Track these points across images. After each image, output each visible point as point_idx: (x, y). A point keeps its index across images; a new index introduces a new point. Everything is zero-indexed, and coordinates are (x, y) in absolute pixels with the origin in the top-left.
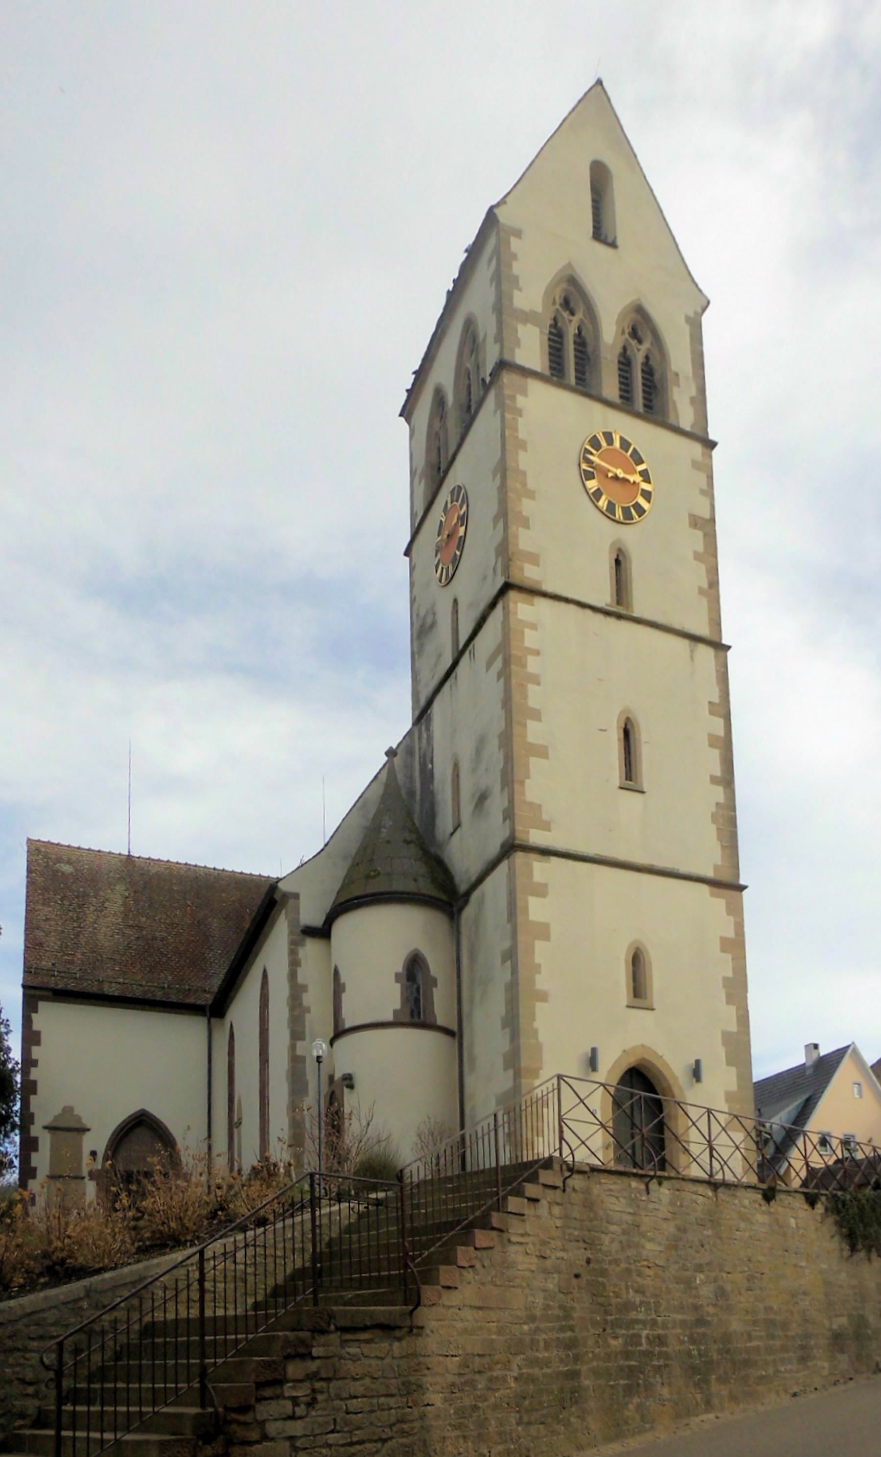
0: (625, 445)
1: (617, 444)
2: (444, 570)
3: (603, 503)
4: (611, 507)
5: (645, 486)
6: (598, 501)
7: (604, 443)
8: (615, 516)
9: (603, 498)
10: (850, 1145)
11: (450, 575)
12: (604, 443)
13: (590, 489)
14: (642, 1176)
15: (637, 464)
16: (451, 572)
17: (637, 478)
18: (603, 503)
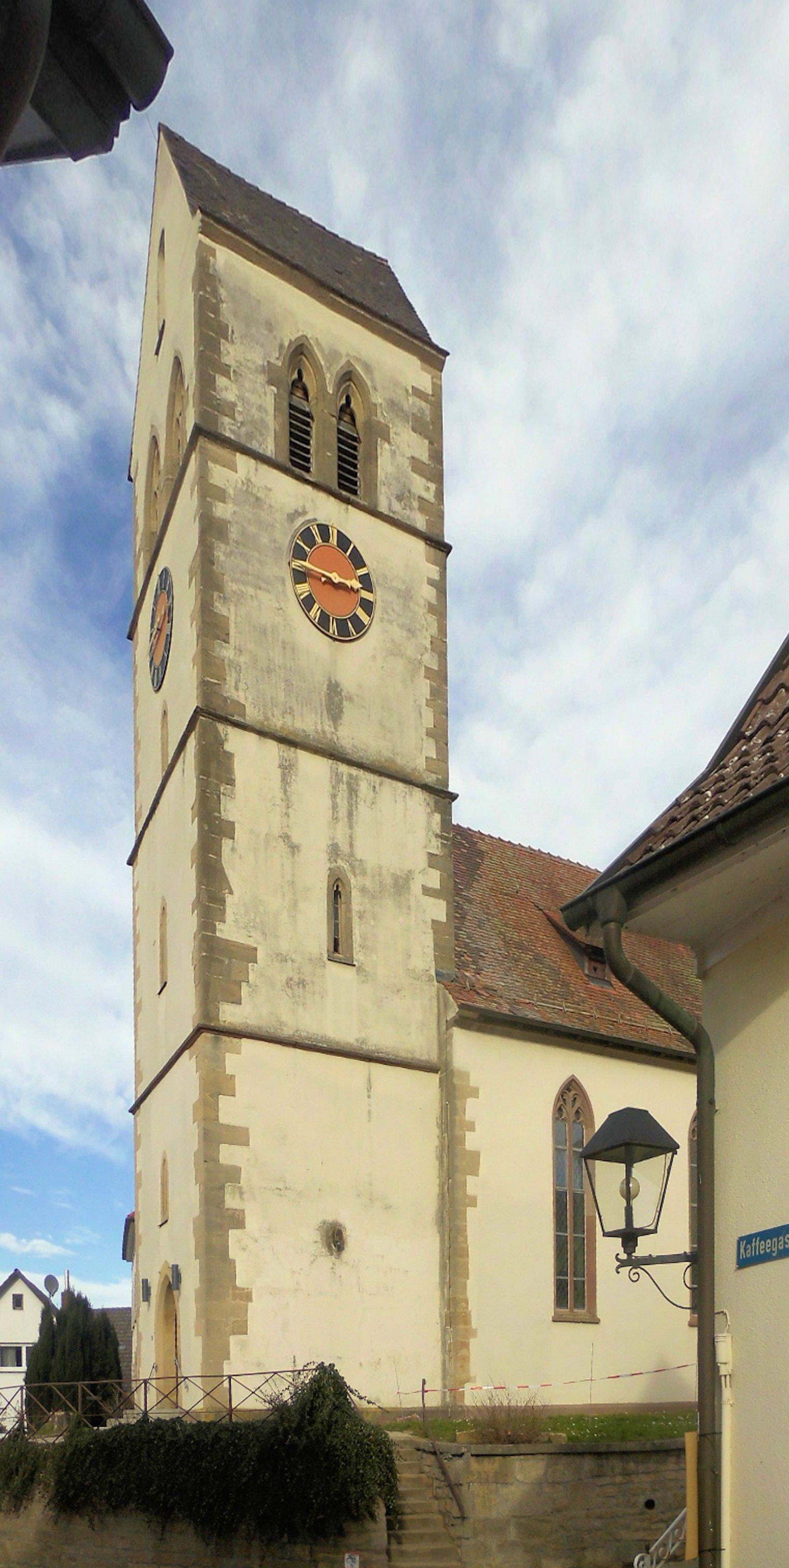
0: (343, 541)
1: (334, 540)
2: (156, 671)
3: (315, 612)
4: (326, 537)
5: (365, 594)
6: (309, 612)
7: (319, 540)
8: (329, 631)
9: (316, 606)
10: (221, 1439)
11: (160, 680)
12: (319, 540)
13: (301, 595)
14: (334, 1236)
15: (357, 568)
16: (161, 676)
17: (357, 585)
18: (315, 612)
